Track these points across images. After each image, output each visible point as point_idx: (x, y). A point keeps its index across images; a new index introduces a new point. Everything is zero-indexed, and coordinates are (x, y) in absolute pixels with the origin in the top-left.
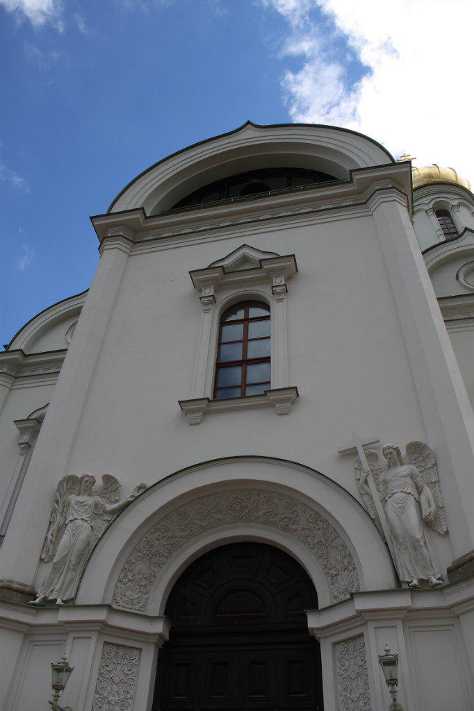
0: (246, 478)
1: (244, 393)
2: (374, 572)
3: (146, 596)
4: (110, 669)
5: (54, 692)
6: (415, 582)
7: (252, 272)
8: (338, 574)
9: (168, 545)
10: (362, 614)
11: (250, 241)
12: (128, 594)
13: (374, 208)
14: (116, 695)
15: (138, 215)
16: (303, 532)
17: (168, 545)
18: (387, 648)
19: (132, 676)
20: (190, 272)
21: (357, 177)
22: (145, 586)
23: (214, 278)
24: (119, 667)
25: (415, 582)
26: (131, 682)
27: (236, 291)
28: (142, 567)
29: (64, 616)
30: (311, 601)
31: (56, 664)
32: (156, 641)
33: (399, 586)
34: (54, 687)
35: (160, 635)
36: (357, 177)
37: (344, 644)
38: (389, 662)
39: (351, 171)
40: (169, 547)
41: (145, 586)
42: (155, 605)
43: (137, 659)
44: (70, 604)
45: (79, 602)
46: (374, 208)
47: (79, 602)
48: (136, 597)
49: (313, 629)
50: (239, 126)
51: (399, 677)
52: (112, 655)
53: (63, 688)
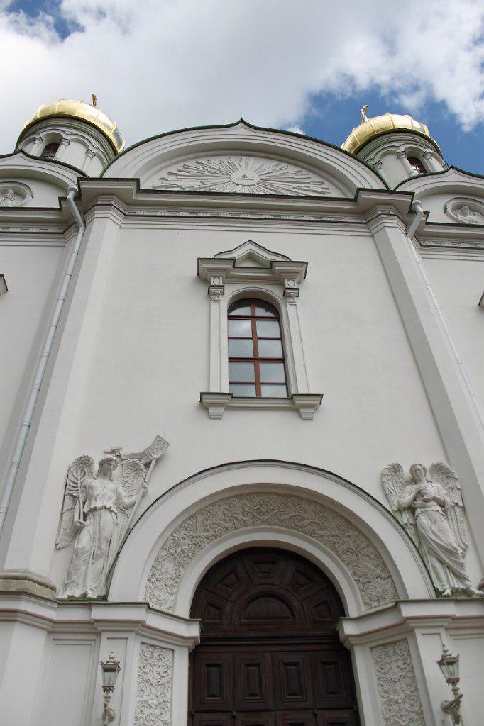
0: (318, 491)
1: (258, 391)
2: (414, 582)
3: (173, 597)
4: (386, 670)
5: (450, 687)
6: (448, 592)
7: (251, 270)
8: (370, 582)
9: (192, 545)
10: (408, 621)
11: (262, 239)
12: (156, 593)
13: (376, 230)
14: (155, 698)
15: (133, 187)
16: (331, 538)
17: (192, 545)
18: (112, 655)
19: (167, 679)
20: (199, 259)
21: (364, 196)
22: (171, 587)
23: (225, 270)
24: (155, 669)
25: (448, 592)
26: (167, 685)
27: (246, 286)
28: (168, 567)
29: (98, 613)
30: (337, 608)
31: (105, 663)
32: (190, 644)
33: (439, 597)
34: (449, 681)
35: (194, 638)
36: (364, 196)
37: (382, 647)
38: (448, 662)
39: (359, 190)
40: (193, 547)
41: (171, 587)
42: (184, 610)
43: (170, 661)
44: (103, 601)
45: (111, 599)
46: (376, 230)
47: (111, 599)
48: (164, 598)
49: (349, 636)
50: (257, 126)
51: (116, 686)
52: (383, 657)
53: (458, 680)
